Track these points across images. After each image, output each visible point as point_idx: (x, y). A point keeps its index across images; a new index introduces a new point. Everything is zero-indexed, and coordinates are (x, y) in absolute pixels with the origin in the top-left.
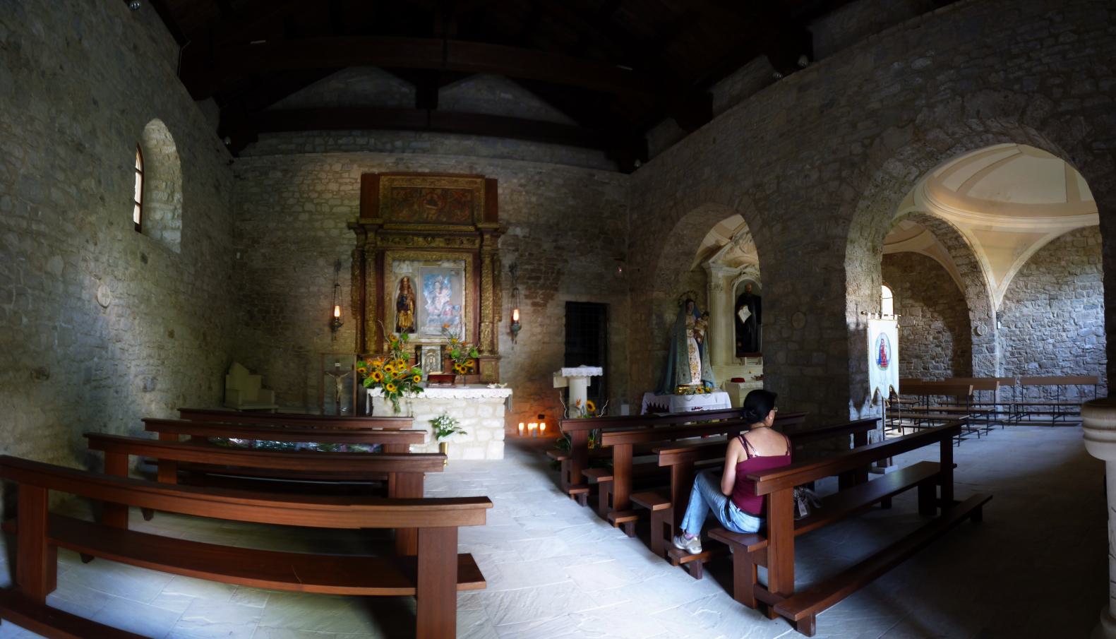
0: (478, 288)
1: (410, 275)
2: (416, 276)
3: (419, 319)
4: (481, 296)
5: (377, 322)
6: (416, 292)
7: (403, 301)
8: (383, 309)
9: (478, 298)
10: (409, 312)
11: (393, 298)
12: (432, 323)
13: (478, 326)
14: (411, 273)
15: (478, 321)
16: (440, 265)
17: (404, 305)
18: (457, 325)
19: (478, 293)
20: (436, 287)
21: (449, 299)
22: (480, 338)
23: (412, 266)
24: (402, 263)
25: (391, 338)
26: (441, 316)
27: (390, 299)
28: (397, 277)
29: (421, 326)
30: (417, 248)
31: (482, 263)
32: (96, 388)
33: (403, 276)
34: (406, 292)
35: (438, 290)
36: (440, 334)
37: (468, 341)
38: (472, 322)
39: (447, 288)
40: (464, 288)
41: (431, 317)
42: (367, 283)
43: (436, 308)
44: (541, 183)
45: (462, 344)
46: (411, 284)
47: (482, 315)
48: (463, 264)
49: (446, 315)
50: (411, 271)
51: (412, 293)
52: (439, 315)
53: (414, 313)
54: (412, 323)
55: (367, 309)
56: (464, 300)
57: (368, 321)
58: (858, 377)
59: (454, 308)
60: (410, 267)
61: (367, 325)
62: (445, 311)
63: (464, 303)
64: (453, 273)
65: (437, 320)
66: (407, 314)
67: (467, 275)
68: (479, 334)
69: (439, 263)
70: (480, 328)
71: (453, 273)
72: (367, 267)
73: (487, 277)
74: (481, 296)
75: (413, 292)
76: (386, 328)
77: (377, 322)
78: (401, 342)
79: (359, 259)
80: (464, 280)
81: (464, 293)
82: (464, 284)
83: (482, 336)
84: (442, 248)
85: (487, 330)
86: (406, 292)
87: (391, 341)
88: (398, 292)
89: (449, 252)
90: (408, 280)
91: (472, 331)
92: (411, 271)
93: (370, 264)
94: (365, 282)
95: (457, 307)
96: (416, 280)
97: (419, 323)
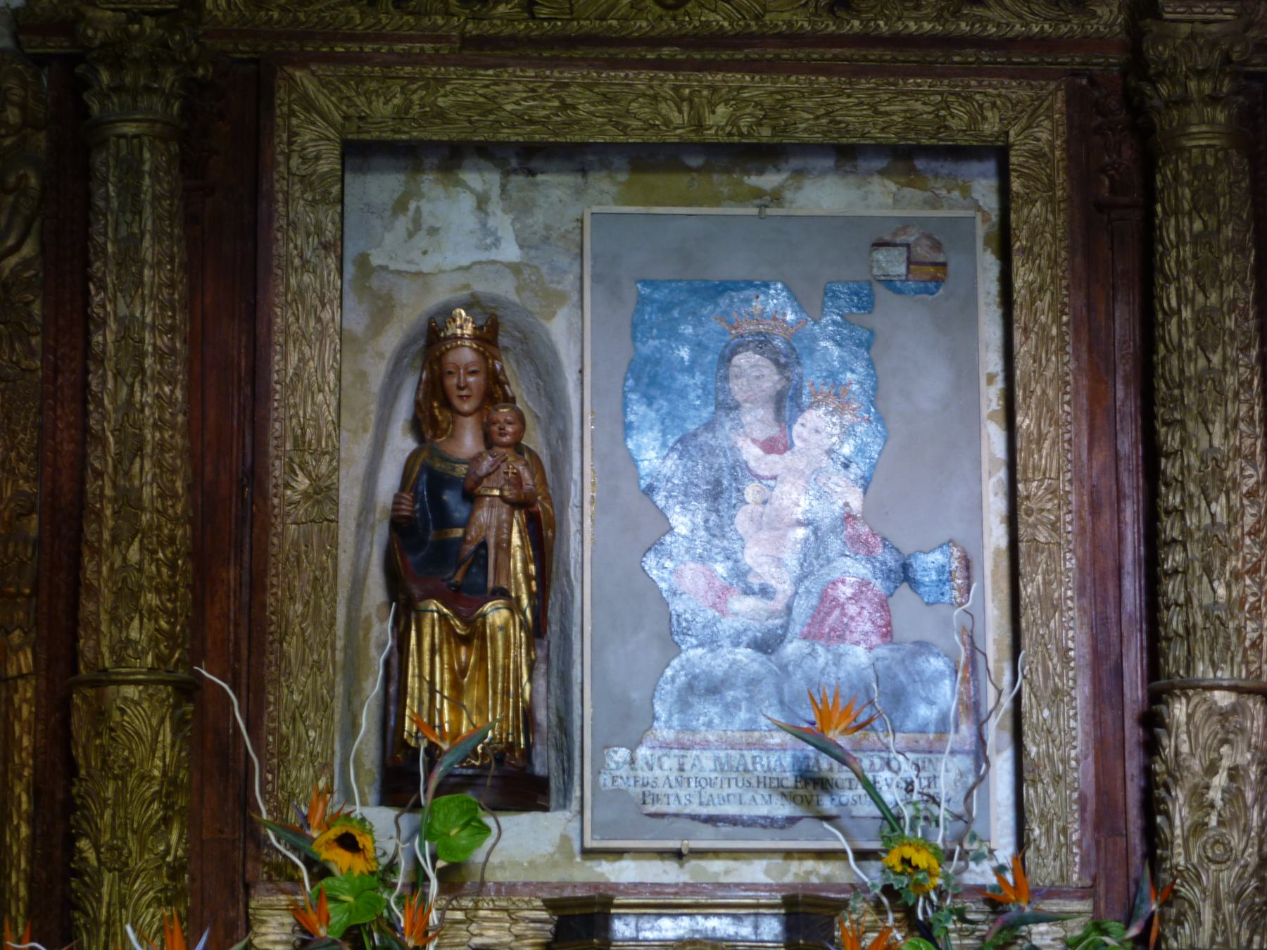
0: (1123, 395)
1: (504, 288)
2: (553, 299)
3: (584, 672)
4: (1152, 453)
5: (189, 689)
6: (560, 461)
7: (443, 518)
8: (256, 584)
9: (1131, 482)
10: (496, 614)
11: (349, 496)
12: (710, 710)
13: (1133, 733)
14: (515, 269)
15: (1134, 691)
16: (776, 197)
17: (445, 553)
18: (943, 726)
19: (1128, 442)
20: (738, 388)
21: (855, 501)
22: (1153, 838)
23: (522, 209)
24: (429, 182)
25: (322, 841)
26: (792, 648)
27: (323, 493)
28: (383, 310)
29: (604, 746)
30: (570, 42)
31: (1148, 163)
32: (636, 782)
33: (440, 295)
34: (468, 442)
35: (757, 420)
36: (782, 809)
37: (1044, 871)
38: (1081, 692)
39: (837, 396)
40: (992, 398)
41: (694, 654)
42: (104, 340)
43: (741, 580)
44: (783, 360)
45: (994, 902)
46: (509, 367)
47: (1175, 620)
48: (985, 190)
49: (839, 634)
50: (510, 252)
51: (517, 447)
52: (766, 644)
53: (537, 631)
54: (528, 718)
55: (98, 572)
56: (996, 505)
57: (102, 680)
58: (988, 891)
59: (904, 574)
60: (501, 221)
61: (100, 715)
62: (827, 601)
63: (996, 536)
64: (893, 263)
65: (753, 683)
66: (475, 635)
67: (1022, 277)
68: (1152, 805)
69: (769, 180)
70: (1151, 747)
71: (893, 263)
72: (110, 192)
73: (1207, 276)
74: (1152, 453)
75: (534, 439)
76: (280, 759)
77: (189, 689)
78: (418, 880)
79: (41, 141)
80: (990, 329)
81: (994, 439)
82: (992, 361)
83: (1180, 812)
84: (793, 39)
85: (1228, 755)
86: (468, 442)
87: (320, 871)
88: (401, 444)
89: (858, 71)
90: (487, 337)
91: (1082, 773)
92: (510, 252)
93: (131, 169)
94: (85, 323)
95: (929, 563)
96: (558, 328)
97: (587, 712)
